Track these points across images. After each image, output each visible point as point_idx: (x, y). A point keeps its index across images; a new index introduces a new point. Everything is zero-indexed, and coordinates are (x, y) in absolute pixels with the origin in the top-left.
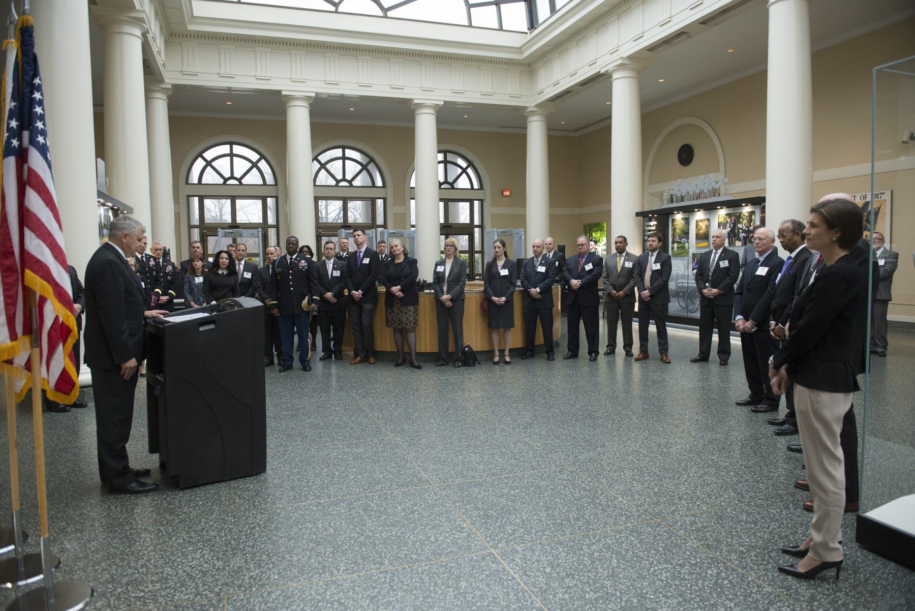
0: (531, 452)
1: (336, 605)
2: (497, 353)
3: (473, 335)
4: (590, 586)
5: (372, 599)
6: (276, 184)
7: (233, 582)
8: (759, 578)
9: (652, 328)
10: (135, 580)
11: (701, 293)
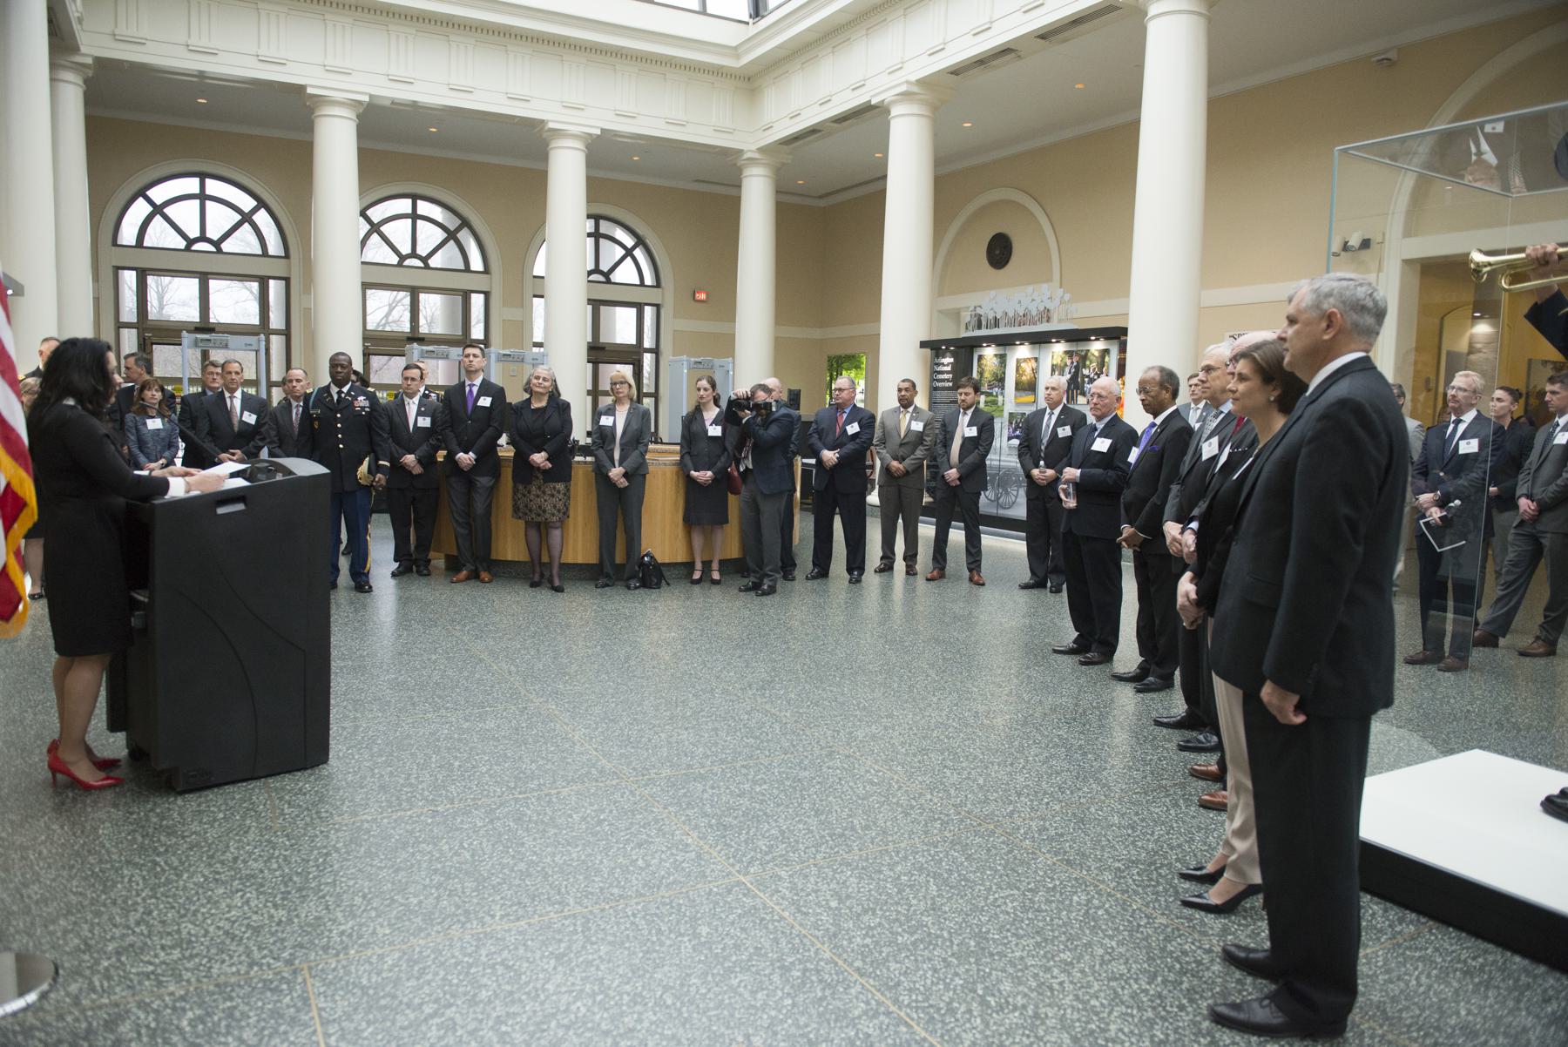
0: (777, 726)
1: (500, 969)
2: (699, 565)
3: (662, 532)
4: (901, 925)
5: (559, 957)
6: (287, 256)
7: (312, 942)
8: (1147, 905)
9: (957, 536)
10: (132, 945)
11: (1029, 476)
